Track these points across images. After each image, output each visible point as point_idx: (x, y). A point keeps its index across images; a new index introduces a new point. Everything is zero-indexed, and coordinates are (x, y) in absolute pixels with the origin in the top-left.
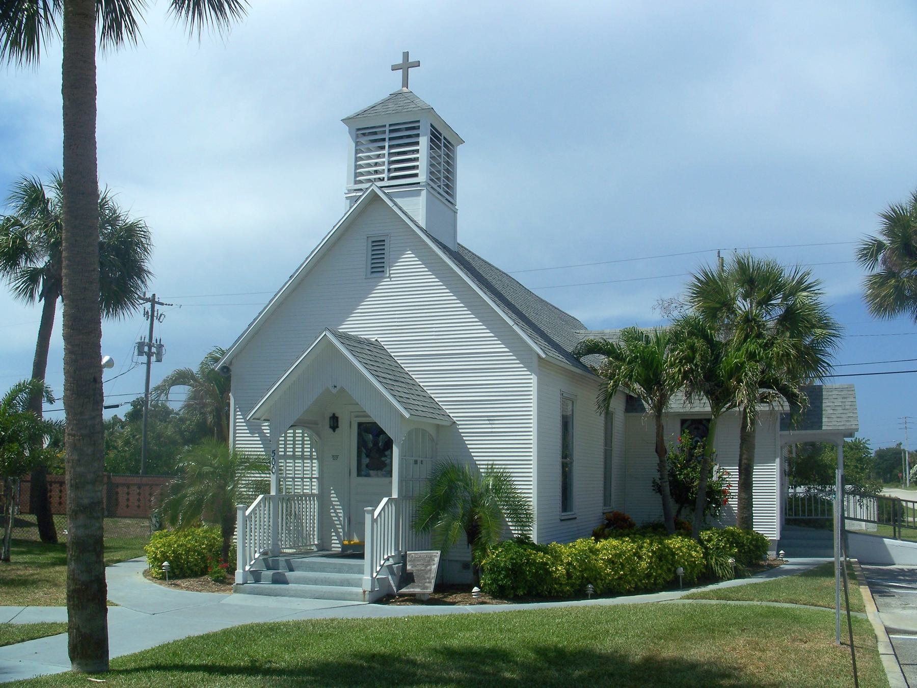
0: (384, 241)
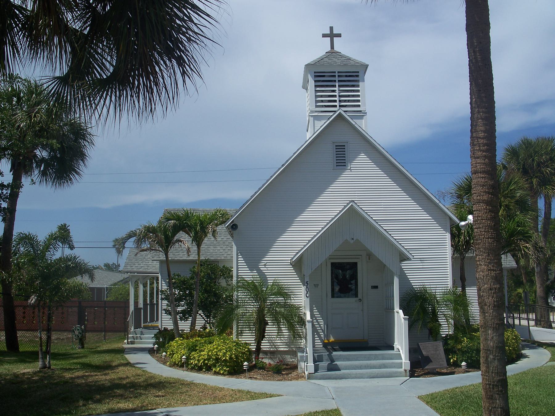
0: (345, 146)
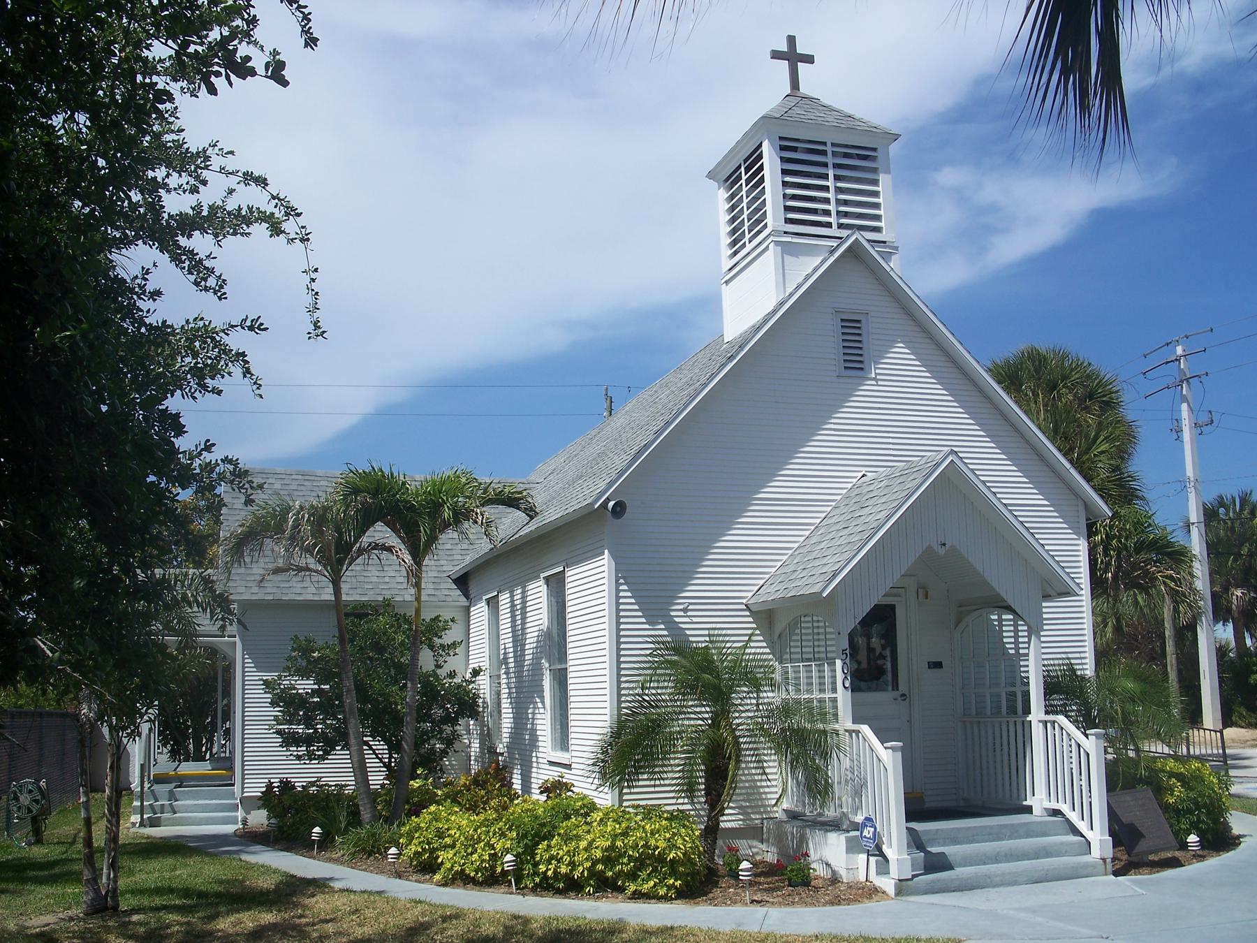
0: (859, 321)
